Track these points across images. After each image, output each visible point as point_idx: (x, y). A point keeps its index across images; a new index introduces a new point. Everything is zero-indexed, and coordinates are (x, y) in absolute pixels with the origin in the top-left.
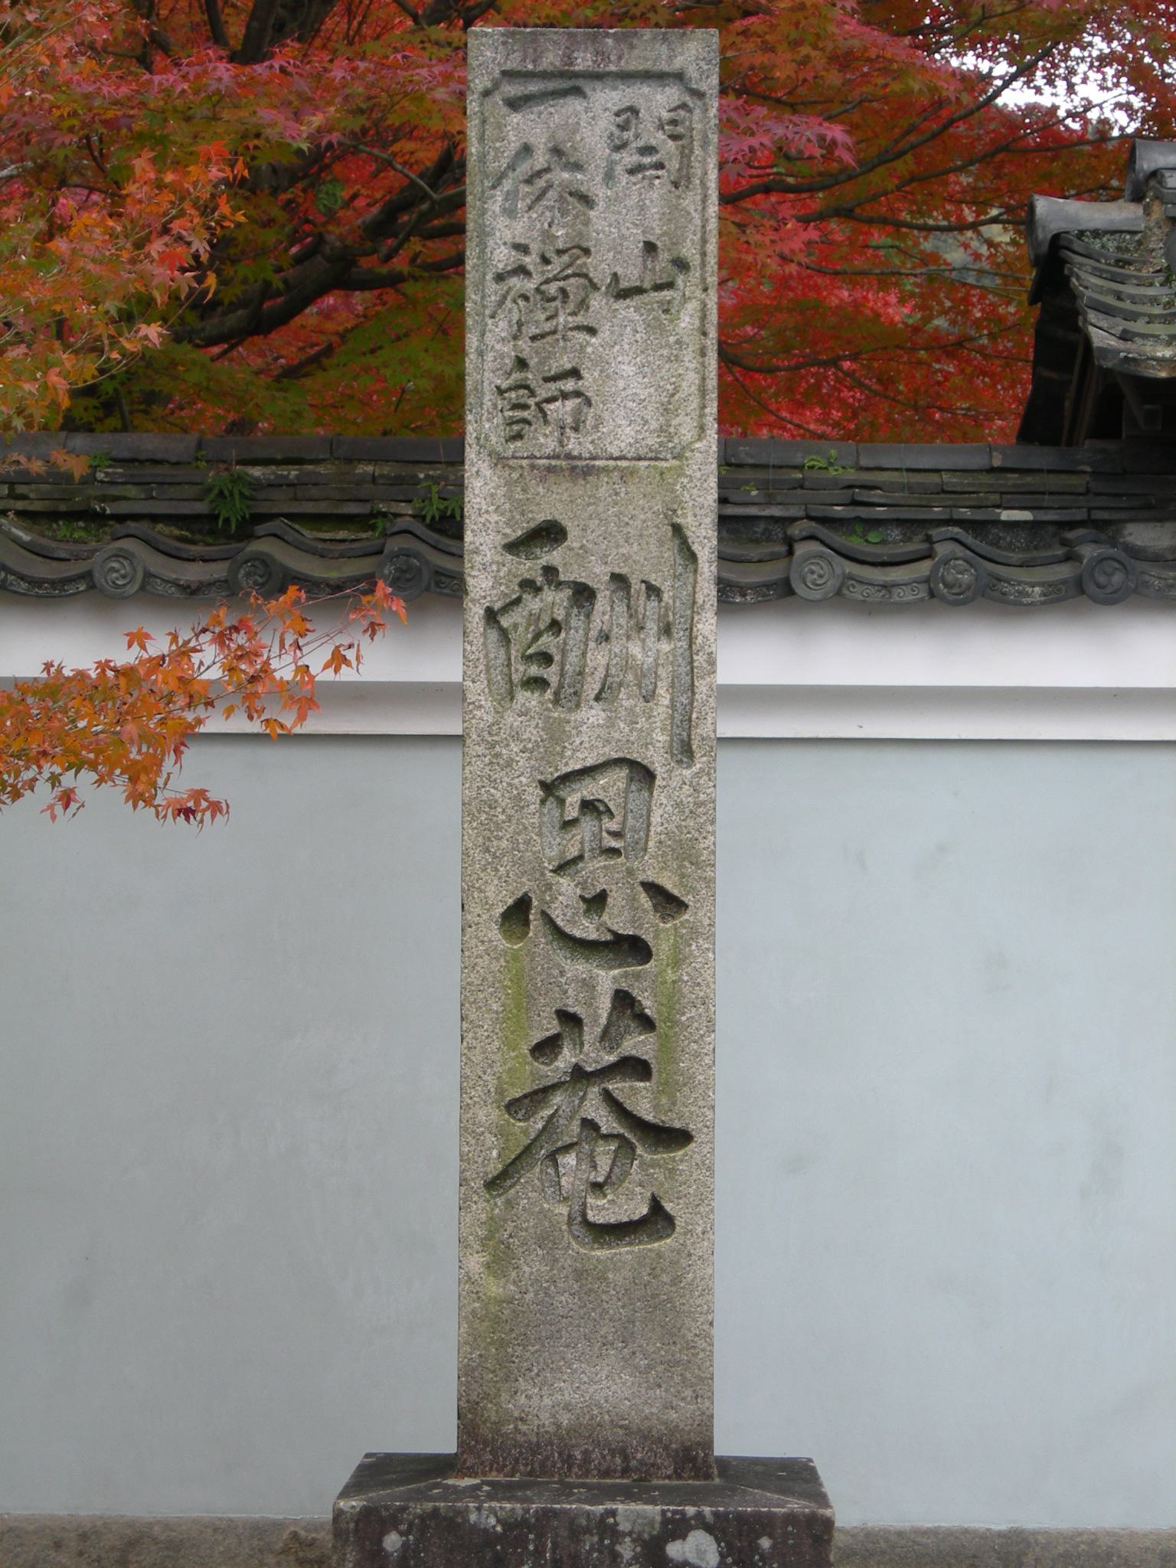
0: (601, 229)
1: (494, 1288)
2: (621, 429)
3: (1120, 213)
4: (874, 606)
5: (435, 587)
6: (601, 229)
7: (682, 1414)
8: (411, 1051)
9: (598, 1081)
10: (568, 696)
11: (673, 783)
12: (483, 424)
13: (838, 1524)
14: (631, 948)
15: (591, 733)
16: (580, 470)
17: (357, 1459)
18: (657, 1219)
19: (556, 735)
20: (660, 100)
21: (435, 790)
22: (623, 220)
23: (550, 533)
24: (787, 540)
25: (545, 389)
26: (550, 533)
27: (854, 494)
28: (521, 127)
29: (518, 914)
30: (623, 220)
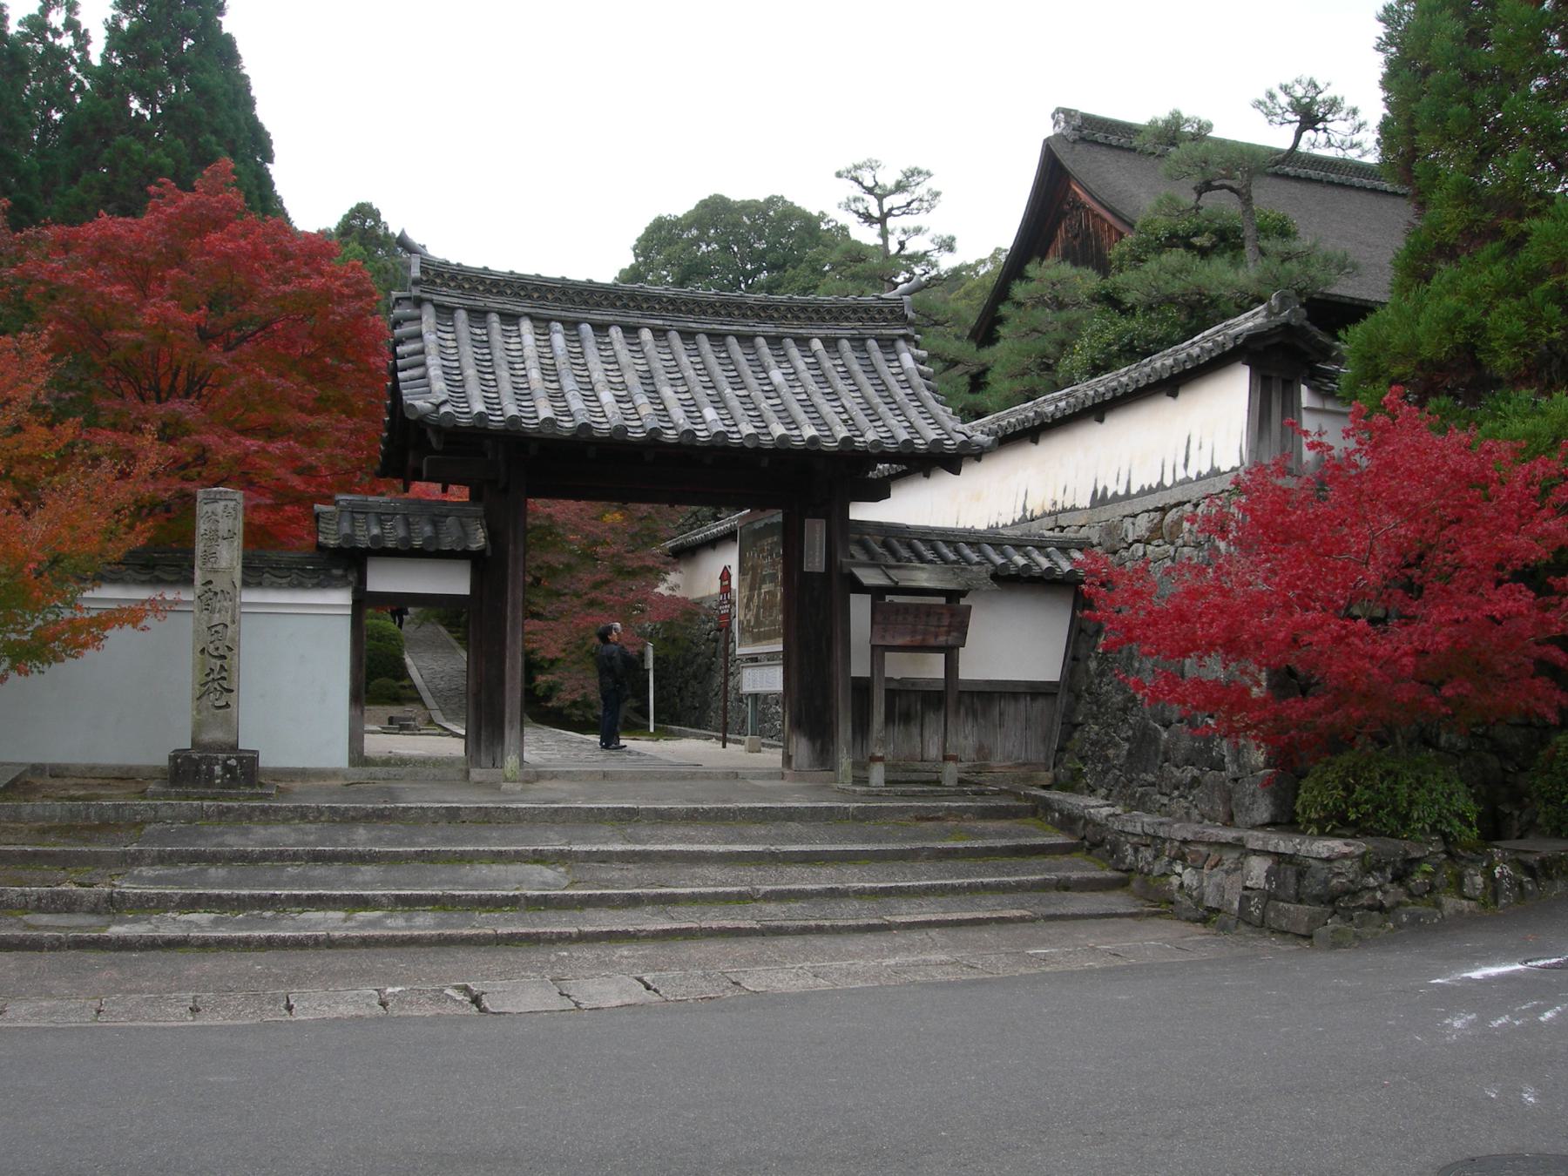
0: (221, 518)
1: (1419, 223)
2: (223, 564)
3: (331, 508)
4: (279, 587)
5: (188, 582)
6: (221, 518)
7: (232, 739)
8: (184, 674)
9: (217, 679)
10: (213, 612)
11: (231, 628)
12: (198, 562)
13: (262, 763)
14: (224, 657)
15: (217, 618)
16: (215, 571)
17: (647, 221)
18: (227, 706)
19: (210, 619)
20: (232, 504)
21: (188, 621)
22: (224, 526)
23: (210, 582)
24: (256, 572)
25: (210, 555)
26: (210, 582)
27: (277, 562)
28: (206, 508)
29: (203, 651)
30: (224, 526)
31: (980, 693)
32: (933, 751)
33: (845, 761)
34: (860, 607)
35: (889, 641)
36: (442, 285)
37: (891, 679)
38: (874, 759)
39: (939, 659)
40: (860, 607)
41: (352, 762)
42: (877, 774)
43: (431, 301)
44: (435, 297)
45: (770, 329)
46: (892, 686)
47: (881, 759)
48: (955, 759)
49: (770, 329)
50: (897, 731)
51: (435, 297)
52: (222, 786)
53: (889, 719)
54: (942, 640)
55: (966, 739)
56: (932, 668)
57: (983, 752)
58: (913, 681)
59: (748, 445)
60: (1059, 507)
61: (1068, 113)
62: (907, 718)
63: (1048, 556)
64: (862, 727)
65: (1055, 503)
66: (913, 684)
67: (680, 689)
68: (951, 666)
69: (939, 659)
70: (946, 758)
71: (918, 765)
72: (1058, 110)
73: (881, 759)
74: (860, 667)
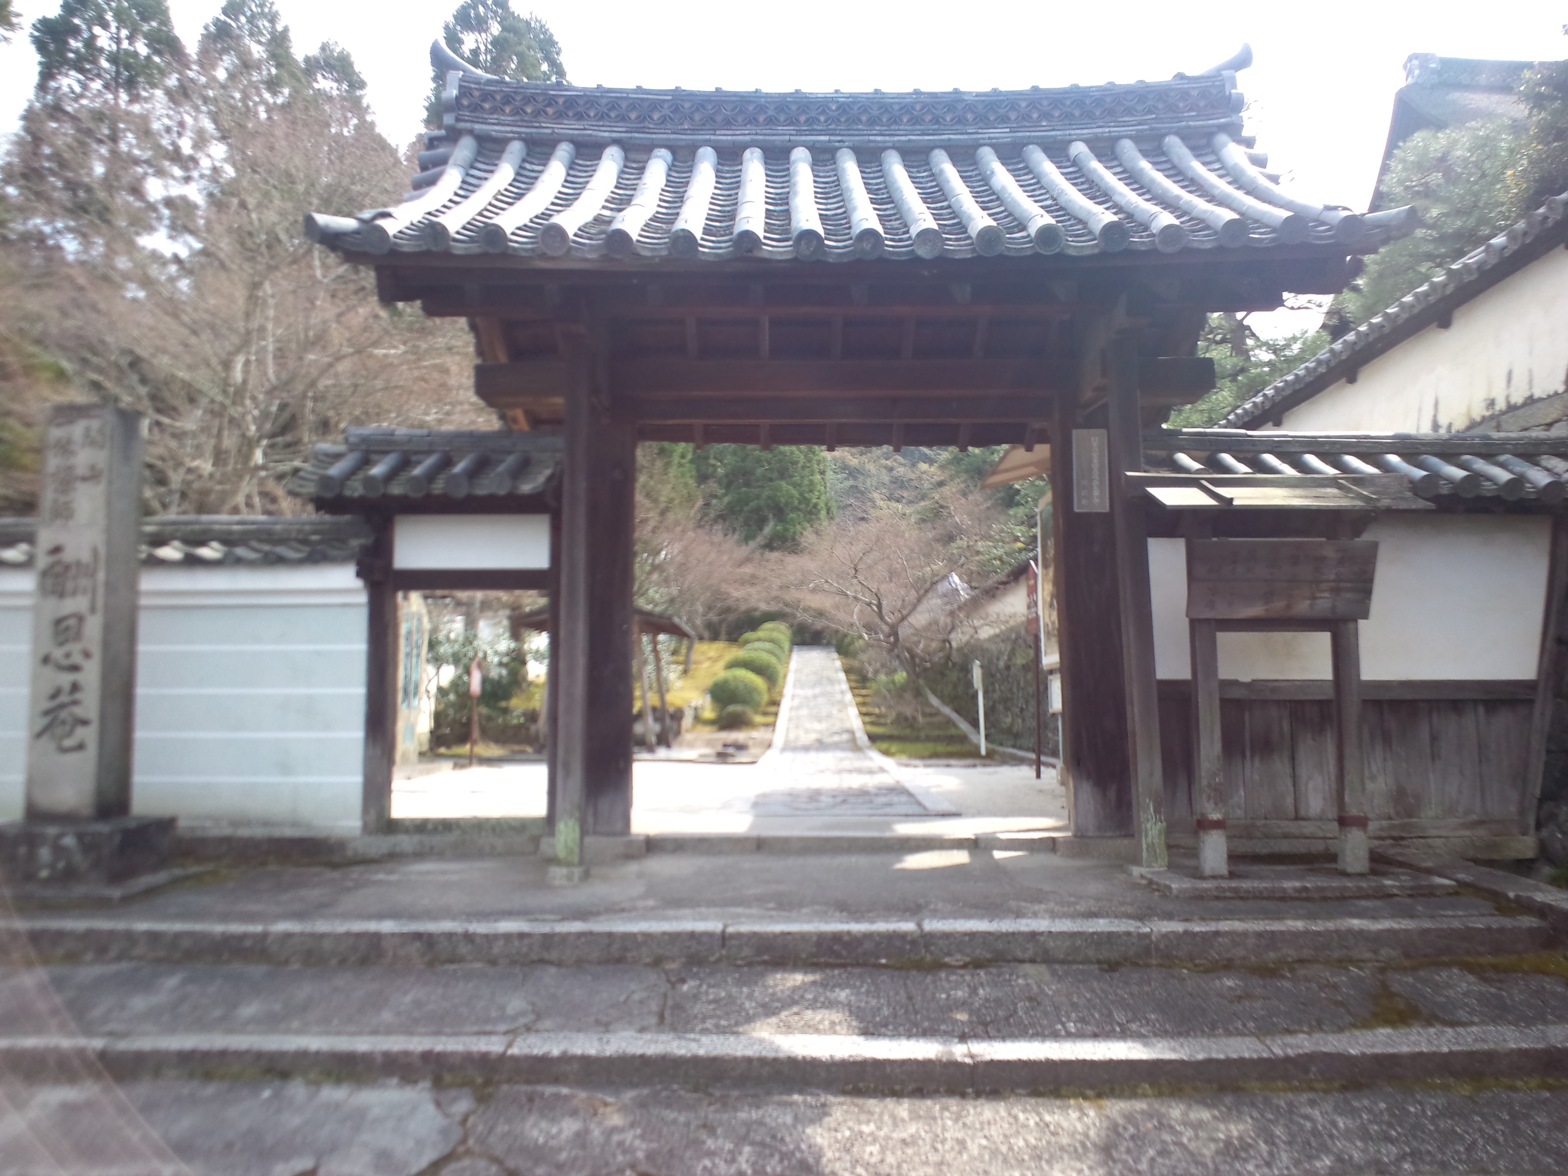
14: (75, 668)
31: (1391, 702)
32: (1316, 799)
33: (1152, 829)
34: (1167, 565)
35: (1222, 612)
36: (494, 110)
37: (1235, 683)
38: (1203, 825)
39: (1320, 643)
40: (1167, 565)
41: (367, 829)
42: (1214, 851)
43: (471, 132)
44: (477, 127)
45: (1001, 133)
46: (1236, 693)
47: (1218, 825)
48: (1362, 822)
49: (1001, 133)
50: (1253, 770)
51: (477, 127)
52: (48, 882)
53: (1232, 746)
54: (1324, 604)
55: (1376, 785)
56: (1308, 660)
57: (1404, 802)
58: (1271, 686)
59: (923, 252)
60: (1501, 405)
61: (1423, 59)
62: (1265, 747)
63: (1503, 466)
64: (1179, 761)
65: (1492, 403)
66: (1274, 690)
67: (1022, 710)
68: (1344, 655)
69: (1320, 643)
70: (1343, 822)
71: (1292, 827)
72: (1415, 56)
73: (1218, 825)
74: (1172, 662)
